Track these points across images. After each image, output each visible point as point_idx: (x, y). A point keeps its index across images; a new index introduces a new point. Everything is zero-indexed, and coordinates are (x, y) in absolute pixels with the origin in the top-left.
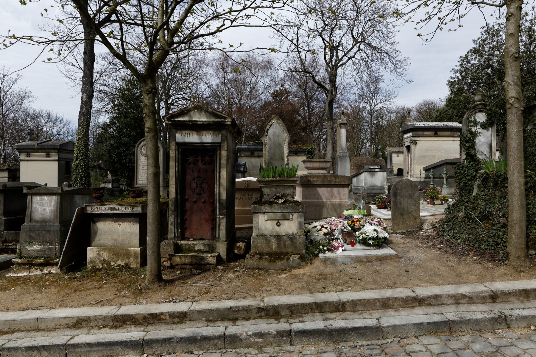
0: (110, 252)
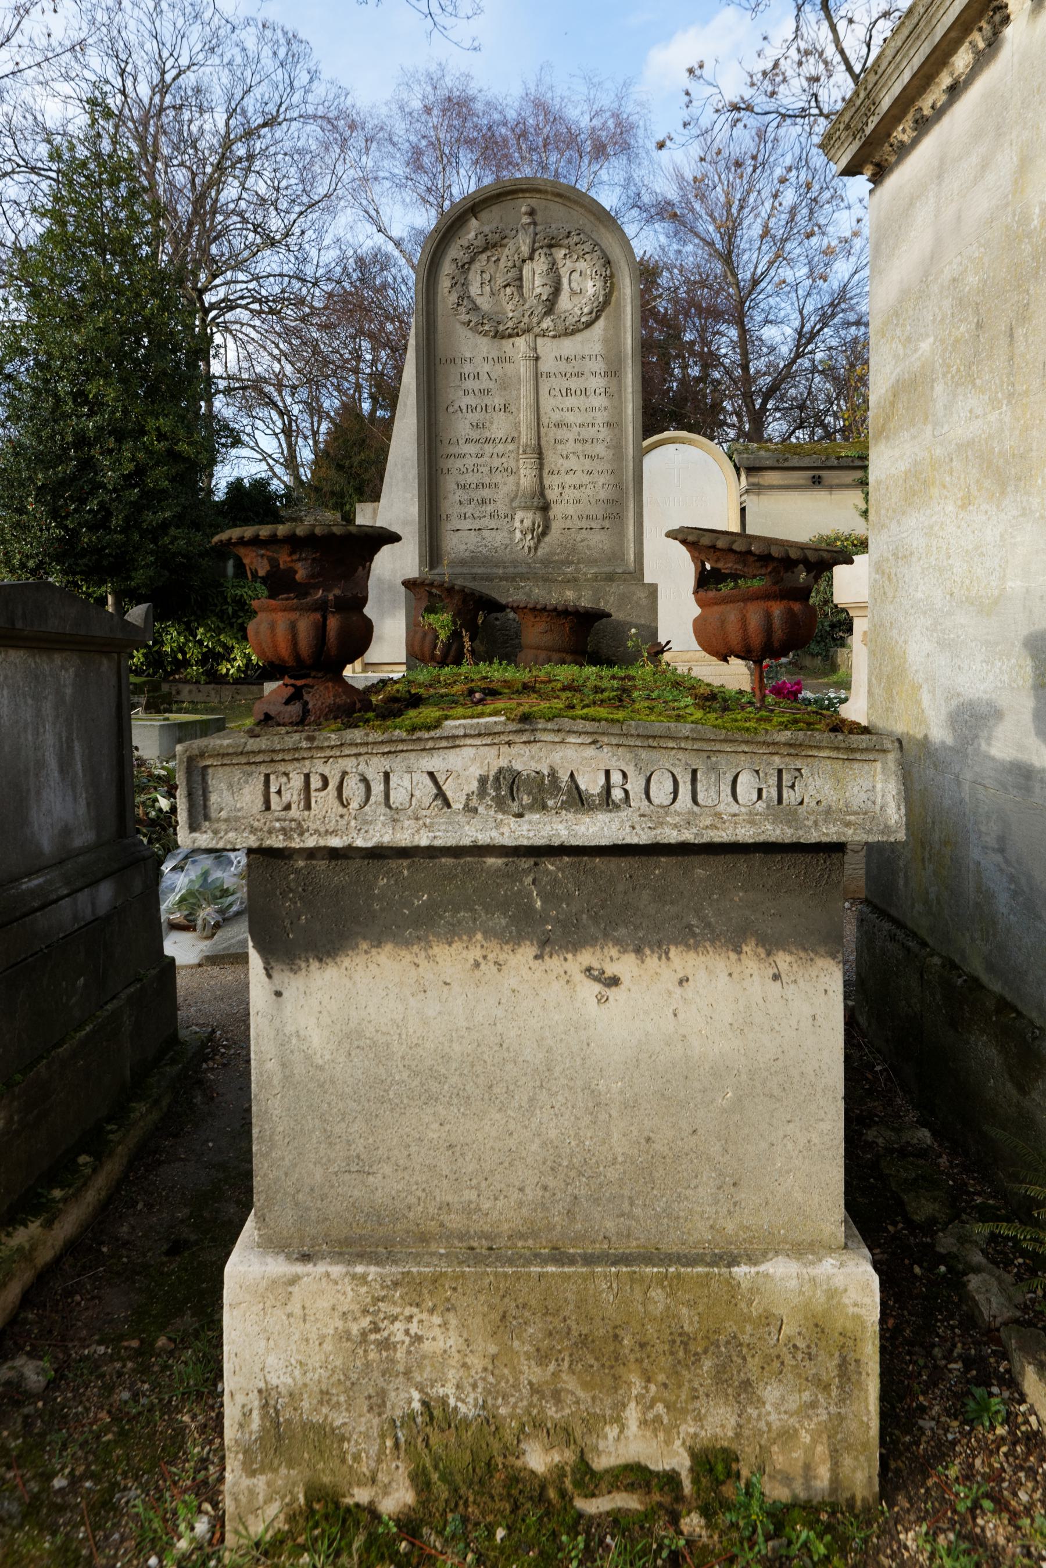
0: (503, 1324)
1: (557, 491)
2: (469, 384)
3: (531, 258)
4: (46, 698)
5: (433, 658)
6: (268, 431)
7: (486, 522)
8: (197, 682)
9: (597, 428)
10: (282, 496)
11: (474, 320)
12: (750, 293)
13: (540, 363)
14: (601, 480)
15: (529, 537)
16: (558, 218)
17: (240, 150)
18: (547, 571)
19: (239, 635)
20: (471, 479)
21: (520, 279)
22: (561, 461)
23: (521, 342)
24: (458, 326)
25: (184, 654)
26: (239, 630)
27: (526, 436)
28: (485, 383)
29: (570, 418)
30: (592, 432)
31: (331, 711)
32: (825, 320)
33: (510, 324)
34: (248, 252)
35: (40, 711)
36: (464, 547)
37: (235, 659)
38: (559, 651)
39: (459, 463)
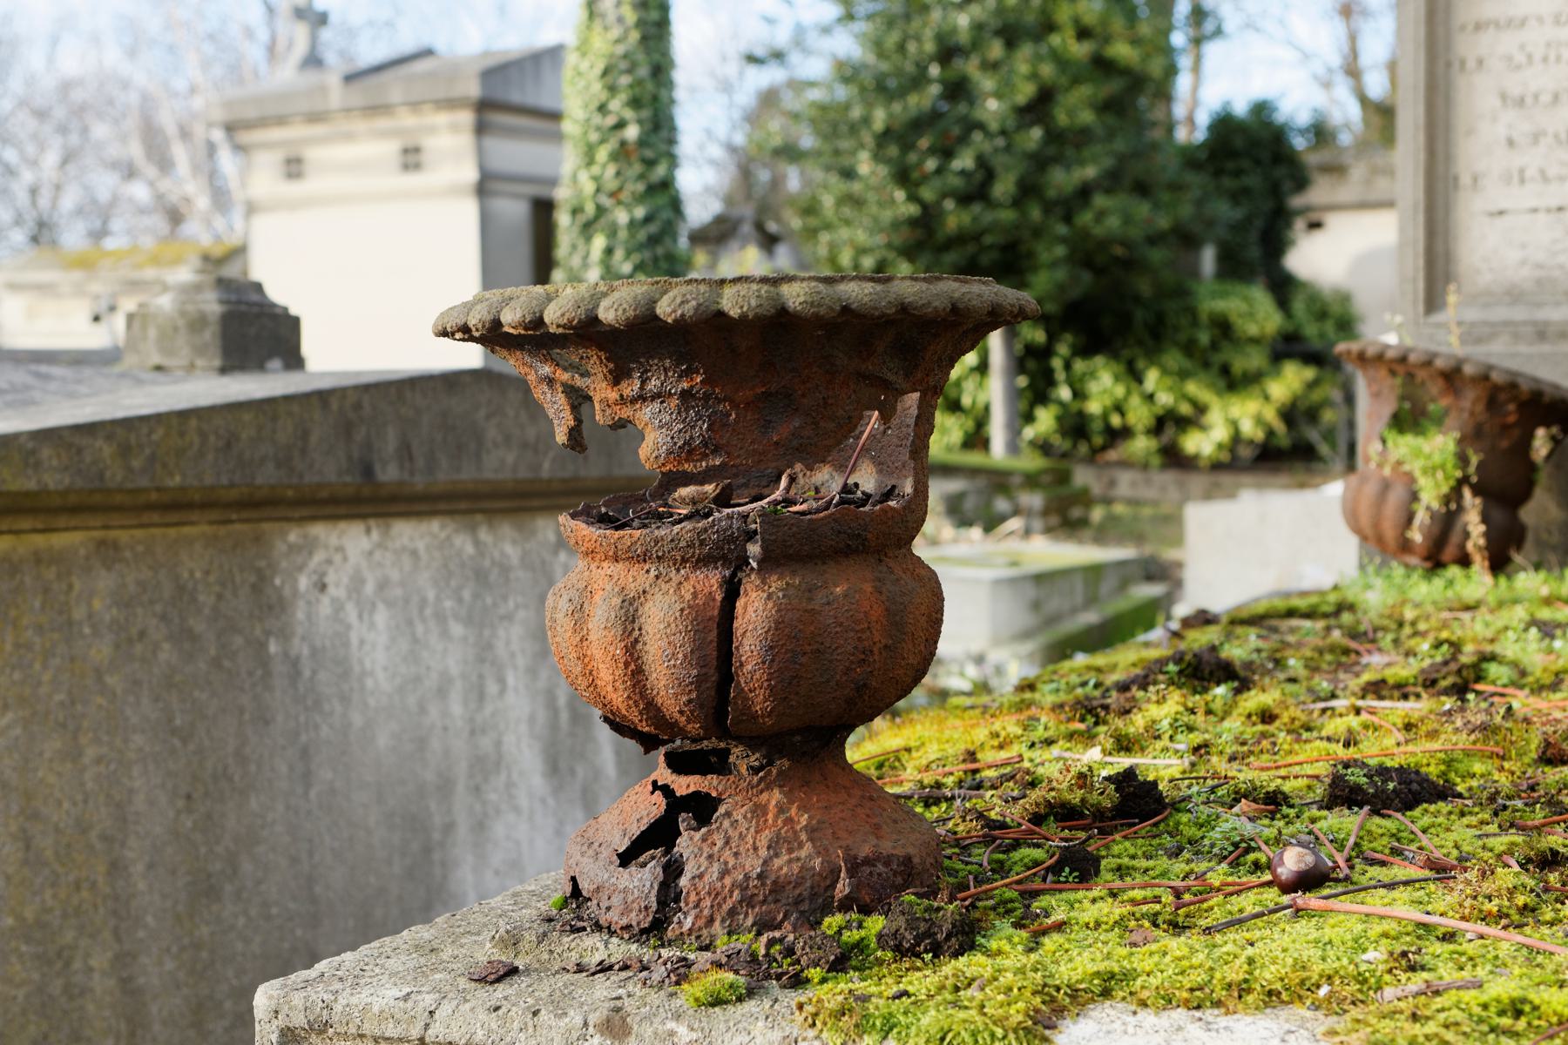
4: (509, 617)
5: (1405, 546)
20: (1539, 80)
31: (748, 901)
35: (489, 646)
39: (1507, 43)
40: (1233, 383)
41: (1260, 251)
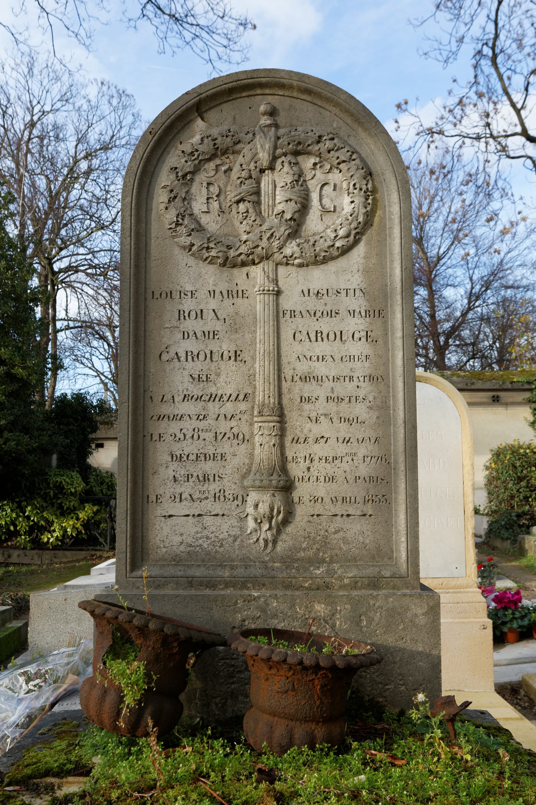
1: (303, 465)
2: (190, 325)
3: (272, 168)
5: (115, 729)
6: (101, 357)
7: (209, 505)
8: (25, 548)
9: (356, 382)
10: (96, 406)
11: (198, 243)
12: (436, 266)
13: (282, 298)
14: (362, 451)
15: (266, 526)
16: (306, 118)
17: (84, 166)
18: (288, 573)
19: (58, 513)
20: (190, 447)
21: (258, 193)
22: (309, 425)
23: (257, 272)
24: (177, 251)
25: (15, 526)
26: (58, 508)
27: (263, 393)
28: (211, 324)
29: (321, 369)
30: (349, 388)
32: (487, 285)
33: (243, 249)
34: (85, 233)
36: (179, 539)
37: (54, 531)
38: (305, 720)
39: (174, 427)
40: (64, 513)
41: (77, 457)
